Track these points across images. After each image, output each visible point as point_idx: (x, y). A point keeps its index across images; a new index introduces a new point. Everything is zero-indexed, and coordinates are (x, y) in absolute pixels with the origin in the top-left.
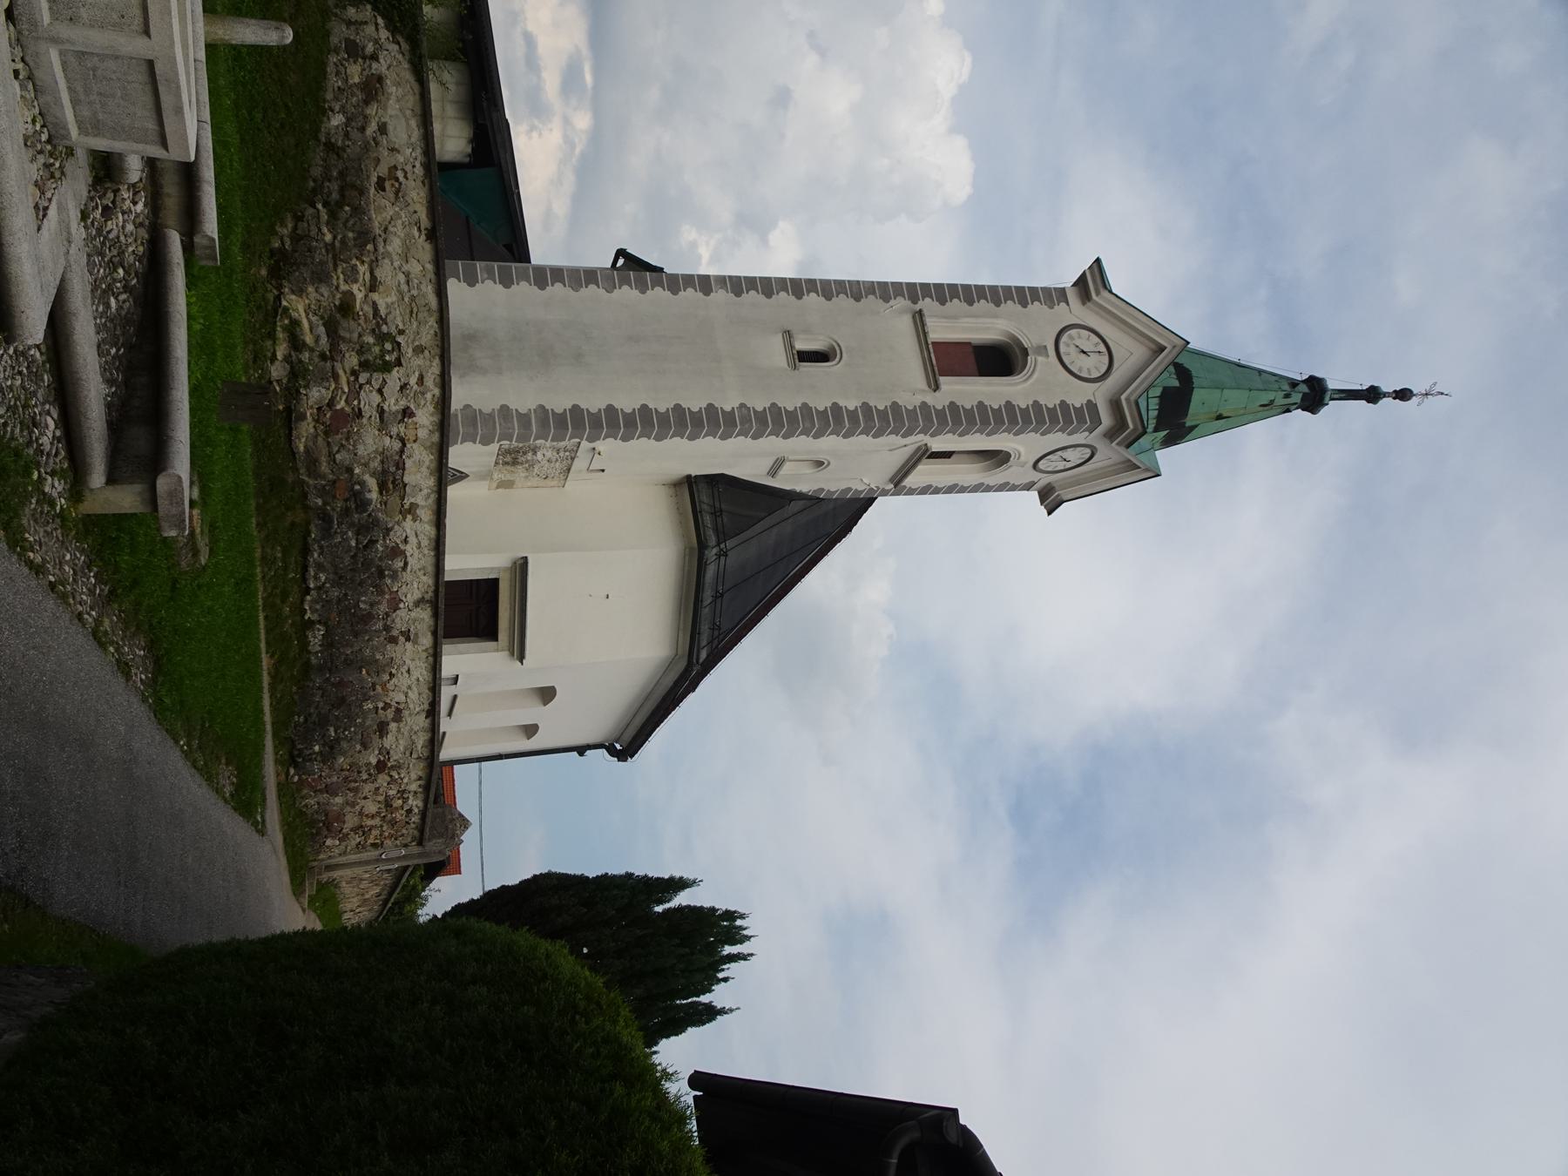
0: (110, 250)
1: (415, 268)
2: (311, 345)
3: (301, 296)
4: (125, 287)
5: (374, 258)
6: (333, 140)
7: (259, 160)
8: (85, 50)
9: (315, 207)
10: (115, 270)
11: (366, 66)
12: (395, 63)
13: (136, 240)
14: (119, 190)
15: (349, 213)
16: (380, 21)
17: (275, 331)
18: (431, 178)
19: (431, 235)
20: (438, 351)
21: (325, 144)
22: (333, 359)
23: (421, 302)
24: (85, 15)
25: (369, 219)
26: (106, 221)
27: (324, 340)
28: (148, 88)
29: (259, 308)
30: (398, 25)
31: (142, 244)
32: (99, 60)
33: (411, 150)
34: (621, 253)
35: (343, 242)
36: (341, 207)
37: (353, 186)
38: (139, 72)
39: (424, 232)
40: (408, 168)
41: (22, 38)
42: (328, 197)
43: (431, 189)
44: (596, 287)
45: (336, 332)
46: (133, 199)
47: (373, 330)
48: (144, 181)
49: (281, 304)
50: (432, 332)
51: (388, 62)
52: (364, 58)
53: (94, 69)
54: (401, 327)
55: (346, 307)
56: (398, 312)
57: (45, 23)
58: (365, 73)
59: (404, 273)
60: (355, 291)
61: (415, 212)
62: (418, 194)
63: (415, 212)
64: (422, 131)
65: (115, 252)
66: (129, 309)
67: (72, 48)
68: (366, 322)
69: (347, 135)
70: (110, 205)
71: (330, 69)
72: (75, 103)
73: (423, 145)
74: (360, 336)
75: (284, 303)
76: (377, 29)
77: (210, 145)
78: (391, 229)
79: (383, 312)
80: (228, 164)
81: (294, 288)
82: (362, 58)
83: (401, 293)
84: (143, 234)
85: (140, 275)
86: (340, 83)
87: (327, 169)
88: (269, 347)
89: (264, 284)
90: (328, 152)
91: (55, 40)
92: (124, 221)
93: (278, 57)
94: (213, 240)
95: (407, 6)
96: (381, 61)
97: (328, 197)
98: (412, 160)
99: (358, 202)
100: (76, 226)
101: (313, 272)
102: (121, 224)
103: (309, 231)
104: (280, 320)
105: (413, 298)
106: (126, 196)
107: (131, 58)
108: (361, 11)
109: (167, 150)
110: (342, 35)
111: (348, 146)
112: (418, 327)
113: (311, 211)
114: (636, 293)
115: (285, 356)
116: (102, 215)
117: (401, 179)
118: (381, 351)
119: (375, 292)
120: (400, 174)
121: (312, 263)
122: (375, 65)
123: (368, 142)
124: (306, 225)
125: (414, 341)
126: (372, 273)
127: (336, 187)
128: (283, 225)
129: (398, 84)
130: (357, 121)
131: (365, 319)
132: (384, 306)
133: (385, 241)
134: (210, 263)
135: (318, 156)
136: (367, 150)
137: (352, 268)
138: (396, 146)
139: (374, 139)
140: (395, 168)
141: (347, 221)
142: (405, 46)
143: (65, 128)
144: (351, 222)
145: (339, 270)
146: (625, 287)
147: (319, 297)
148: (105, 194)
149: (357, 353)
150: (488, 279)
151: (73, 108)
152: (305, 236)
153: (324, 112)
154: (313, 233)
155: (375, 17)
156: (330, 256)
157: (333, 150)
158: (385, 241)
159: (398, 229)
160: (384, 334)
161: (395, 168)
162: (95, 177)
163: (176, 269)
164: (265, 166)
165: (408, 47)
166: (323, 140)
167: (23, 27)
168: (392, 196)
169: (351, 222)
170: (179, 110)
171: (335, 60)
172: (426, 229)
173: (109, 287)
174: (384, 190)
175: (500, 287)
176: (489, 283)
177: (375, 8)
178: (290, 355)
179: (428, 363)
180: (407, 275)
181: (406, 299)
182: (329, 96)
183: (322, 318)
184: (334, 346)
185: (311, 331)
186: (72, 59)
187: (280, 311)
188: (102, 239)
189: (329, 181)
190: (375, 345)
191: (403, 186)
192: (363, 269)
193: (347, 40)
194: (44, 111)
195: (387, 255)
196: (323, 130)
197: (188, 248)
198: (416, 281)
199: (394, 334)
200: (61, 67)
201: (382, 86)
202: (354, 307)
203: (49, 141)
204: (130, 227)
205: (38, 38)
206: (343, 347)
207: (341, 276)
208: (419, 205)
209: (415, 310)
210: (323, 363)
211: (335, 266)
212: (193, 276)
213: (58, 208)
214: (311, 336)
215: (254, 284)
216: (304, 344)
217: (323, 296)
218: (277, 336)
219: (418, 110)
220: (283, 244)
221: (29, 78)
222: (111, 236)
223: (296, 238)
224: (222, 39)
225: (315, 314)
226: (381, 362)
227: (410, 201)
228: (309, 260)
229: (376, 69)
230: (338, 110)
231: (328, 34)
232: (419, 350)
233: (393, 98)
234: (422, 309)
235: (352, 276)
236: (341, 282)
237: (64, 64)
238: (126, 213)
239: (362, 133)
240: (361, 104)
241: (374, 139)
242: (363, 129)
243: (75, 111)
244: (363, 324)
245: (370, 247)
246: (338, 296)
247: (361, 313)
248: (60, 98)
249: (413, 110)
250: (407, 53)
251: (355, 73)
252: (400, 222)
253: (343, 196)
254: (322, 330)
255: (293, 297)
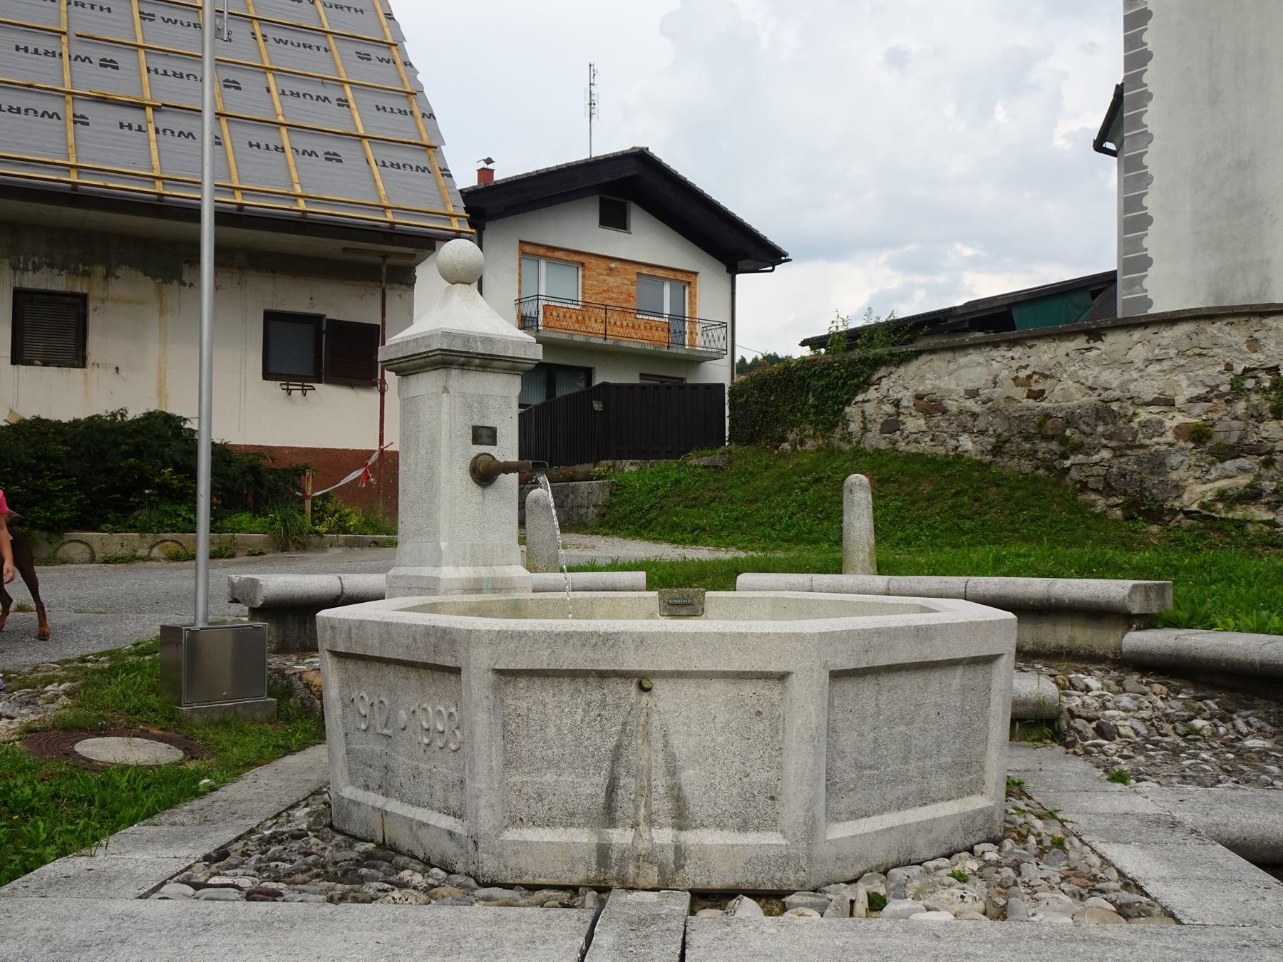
0: (1166, 735)
1: (1139, 353)
2: (1252, 478)
3: (1184, 488)
4: (1223, 720)
5: (1130, 401)
6: (989, 447)
7: (1017, 526)
8: (823, 782)
9: (1069, 469)
10: (1198, 732)
11: (906, 412)
12: (901, 382)
13: (1145, 694)
14: (1069, 710)
15: (1074, 430)
16: (859, 398)
17: (1233, 520)
18: (1025, 339)
19: (1095, 334)
20: (1254, 321)
21: (994, 456)
22: (1271, 452)
23: (1184, 344)
24: (764, 776)
25: (1080, 407)
26: (1120, 736)
27: (1243, 462)
28: (887, 681)
29: (1203, 537)
30: (861, 379)
31: (1147, 684)
32: (842, 759)
33: (994, 362)
34: (1099, 147)
35: (1110, 437)
36: (1068, 439)
37: (1041, 425)
38: (857, 695)
39: (1092, 344)
40: (1015, 364)
41: (814, 882)
42: (1056, 454)
43: (1038, 337)
44: (1146, 156)
45: (1232, 448)
46: (1082, 691)
47: (1227, 402)
48: (1053, 672)
49: (1196, 512)
50: (1227, 329)
51: (900, 389)
52: (898, 414)
53: (860, 767)
54: (1222, 368)
55: (1198, 435)
56: (1200, 372)
57: (784, 842)
58: (914, 413)
59: (1146, 366)
60: (1174, 423)
61: (1067, 355)
62: (1045, 352)
63: (1067, 355)
64: (971, 351)
65: (1167, 728)
66: (1261, 718)
67: (822, 804)
68: (1216, 411)
69: (982, 432)
70: (1094, 724)
71: (913, 449)
72: (925, 799)
73: (989, 349)
74: (1236, 418)
75: (1195, 507)
76: (868, 401)
77: (996, 579)
78: (1090, 383)
79: (1202, 391)
80: (1022, 560)
81: (1174, 495)
82: (899, 416)
83: (1174, 369)
84: (1133, 680)
85: (1199, 694)
86: (927, 439)
87: (1022, 454)
88: (1257, 528)
89: (1170, 530)
90: (1003, 453)
91: (811, 831)
92: (1117, 708)
93: (904, 500)
94: (1135, 587)
95: (842, 370)
96: (900, 396)
97: (1056, 454)
98: (1005, 361)
99: (1060, 420)
100: (1139, 799)
101: (1152, 473)
102: (1123, 714)
103: (1098, 475)
104: (1218, 513)
105: (1181, 354)
106: (1078, 701)
107: (831, 704)
108: (852, 417)
109: (999, 656)
110: (878, 437)
111: (995, 431)
112: (1221, 347)
113: (1074, 474)
114: (1151, 106)
115: (1268, 510)
116: (1111, 739)
117: (1028, 372)
118: (1257, 392)
119: (1174, 400)
120: (1023, 374)
121: (1140, 473)
122: (904, 403)
123: (989, 409)
124: (1091, 479)
125: (1240, 351)
126: (1149, 404)
127: (1044, 444)
128: (1093, 504)
129: (922, 378)
130: (966, 422)
131: (1211, 411)
132: (1192, 389)
133: (1107, 389)
134: (1170, 594)
135: (1009, 465)
136: (998, 410)
137: (1142, 427)
138: (991, 378)
139: (984, 403)
140: (1015, 379)
141: (1083, 432)
142: (883, 371)
143: (972, 816)
144: (1085, 428)
145: (1147, 442)
146: (1145, 120)
147: (1185, 466)
148: (1079, 732)
149: (1260, 422)
150: (1141, 285)
151: (934, 801)
152: (1105, 479)
153: (959, 456)
154: (1102, 471)
155: (856, 403)
156: (1129, 452)
157: (1000, 447)
158: (1107, 389)
159: (1090, 374)
160: (1232, 389)
161: (1015, 379)
162: (1053, 740)
163: (1186, 643)
164: (1024, 521)
165: (883, 369)
166: (989, 458)
167: (792, 878)
168: (1049, 382)
169: (1085, 428)
170: (922, 633)
171: (903, 444)
172: (1088, 341)
173: (1229, 745)
174: (1042, 392)
175: (1151, 271)
176: (1146, 283)
177: (848, 403)
178: (1268, 503)
179: (1272, 333)
180: (1149, 362)
181: (1183, 362)
182: (941, 451)
183: (1212, 463)
184: (1253, 450)
185: (1231, 477)
186: (843, 804)
187: (1205, 512)
188: (1149, 746)
189: (1036, 452)
190: (1248, 400)
191: (1037, 370)
192: (1144, 414)
193: (882, 431)
194: (944, 850)
195: (1124, 386)
196: (978, 458)
197: (1148, 621)
198: (1157, 351)
199: (1232, 377)
200: (862, 821)
201: (925, 395)
202: (1197, 425)
203: (997, 841)
204: (1125, 700)
205: (809, 858)
206: (1253, 439)
207: (1155, 439)
208: (1058, 351)
209: (1197, 351)
210: (1277, 465)
211: (1142, 446)
212: (1191, 618)
213: (1116, 841)
214: (1239, 477)
215: (1172, 541)
216: (1250, 486)
217: (1182, 462)
218: (1241, 517)
219: (949, 355)
220: (1117, 505)
221: (885, 873)
222: (1143, 731)
223: (1108, 490)
224: (870, 555)
225: (1207, 471)
226: (1273, 393)
227: (1055, 361)
228: (1136, 477)
229: (909, 402)
230: (956, 442)
231: (878, 451)
232: (1254, 344)
233: (937, 383)
234: (1195, 342)
235: (1155, 428)
236: (1162, 440)
237: (855, 815)
238: (1103, 704)
239: (978, 416)
240: (948, 417)
241: (984, 403)
242: (974, 415)
243: (942, 799)
244: (1219, 415)
245: (1115, 406)
246: (1182, 443)
247: (1204, 417)
248: (918, 823)
249: (949, 362)
250: (890, 369)
251: (914, 423)
252: (1080, 373)
253: (1052, 438)
254: (1230, 465)
255: (1185, 497)
